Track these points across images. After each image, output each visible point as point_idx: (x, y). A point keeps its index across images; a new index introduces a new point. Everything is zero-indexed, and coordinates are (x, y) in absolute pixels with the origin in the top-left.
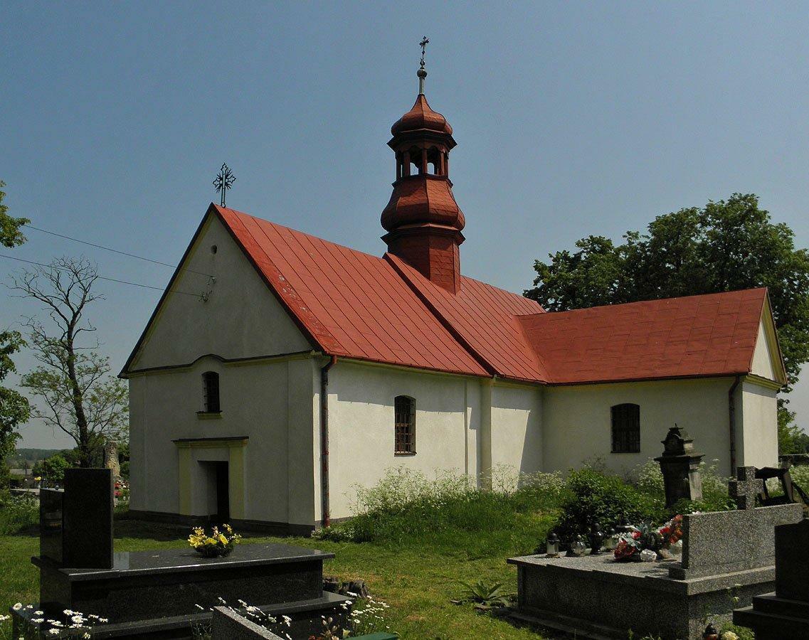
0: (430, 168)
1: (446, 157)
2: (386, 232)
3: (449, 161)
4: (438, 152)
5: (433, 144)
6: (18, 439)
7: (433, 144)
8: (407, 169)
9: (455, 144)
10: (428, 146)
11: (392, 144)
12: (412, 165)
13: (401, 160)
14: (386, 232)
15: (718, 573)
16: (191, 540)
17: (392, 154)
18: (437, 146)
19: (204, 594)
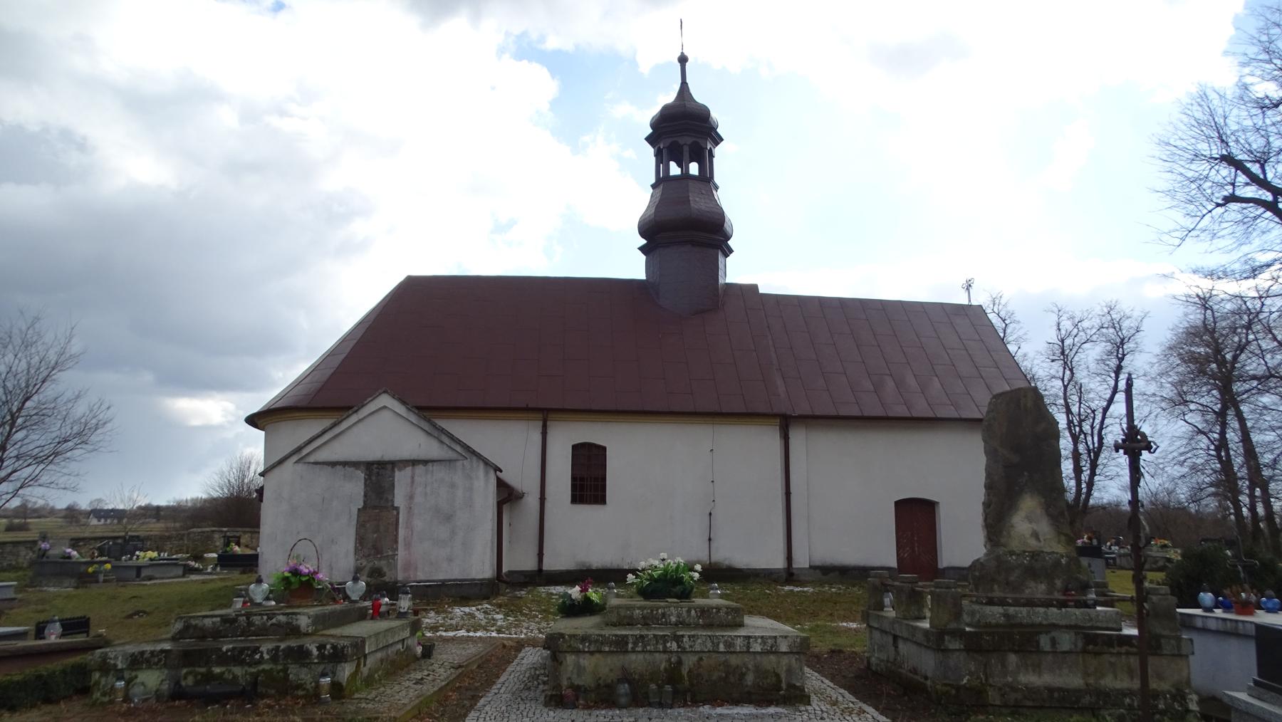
0: (694, 168)
1: (711, 155)
2: (644, 242)
3: (715, 160)
4: (703, 149)
5: (694, 139)
6: (76, 585)
7: (694, 139)
8: (667, 169)
9: (900, 505)
10: (689, 140)
11: (651, 140)
12: (673, 165)
13: (661, 158)
14: (644, 242)
15: (203, 532)
16: (1175, 555)
17: (650, 151)
18: (698, 140)
19: (959, 590)
